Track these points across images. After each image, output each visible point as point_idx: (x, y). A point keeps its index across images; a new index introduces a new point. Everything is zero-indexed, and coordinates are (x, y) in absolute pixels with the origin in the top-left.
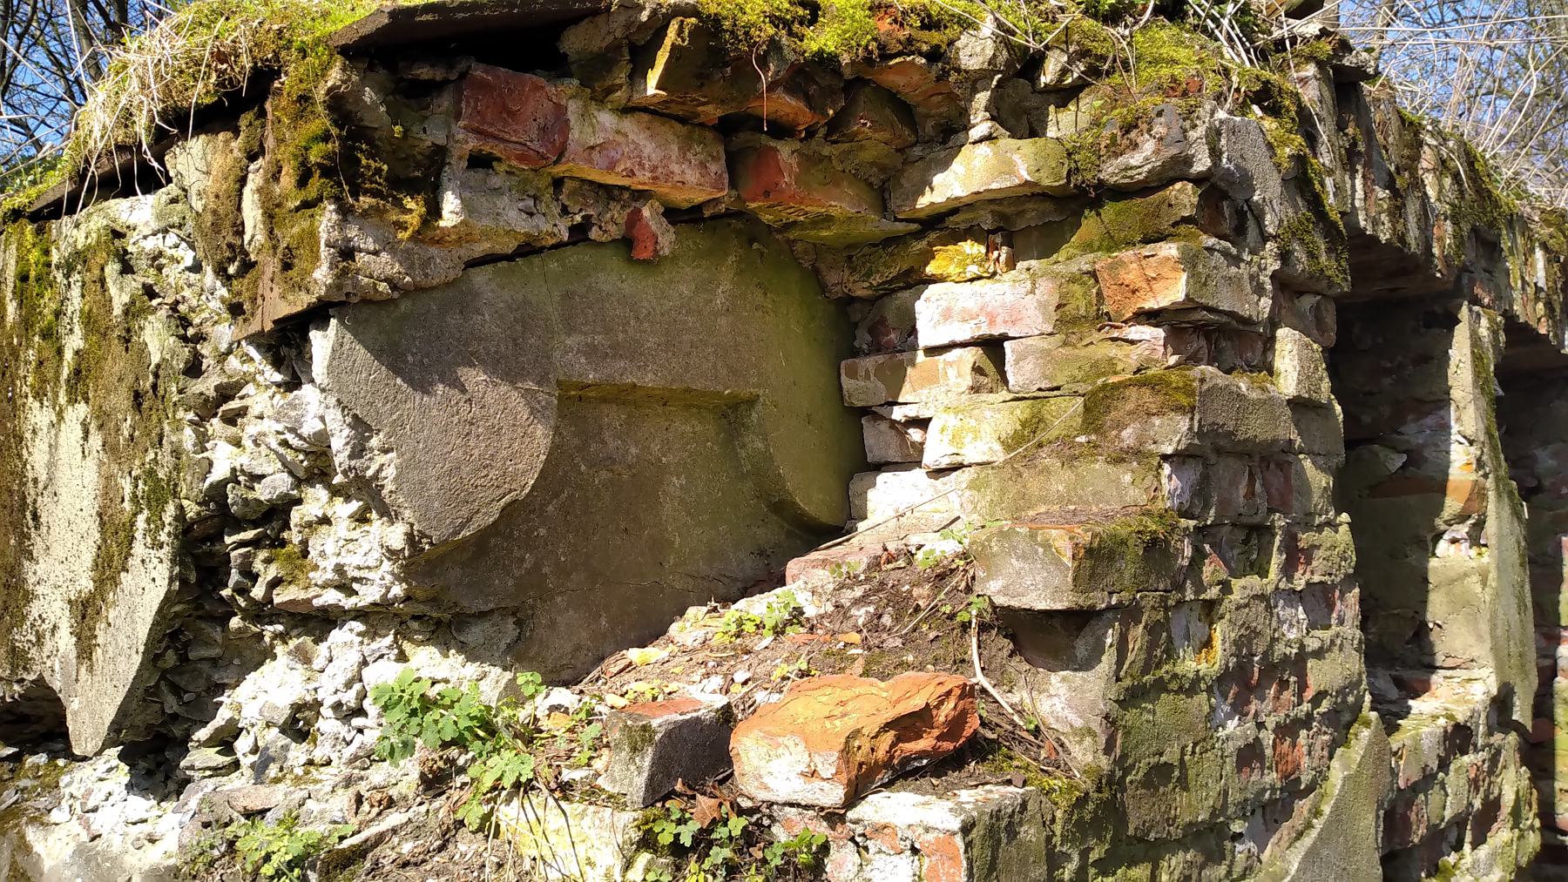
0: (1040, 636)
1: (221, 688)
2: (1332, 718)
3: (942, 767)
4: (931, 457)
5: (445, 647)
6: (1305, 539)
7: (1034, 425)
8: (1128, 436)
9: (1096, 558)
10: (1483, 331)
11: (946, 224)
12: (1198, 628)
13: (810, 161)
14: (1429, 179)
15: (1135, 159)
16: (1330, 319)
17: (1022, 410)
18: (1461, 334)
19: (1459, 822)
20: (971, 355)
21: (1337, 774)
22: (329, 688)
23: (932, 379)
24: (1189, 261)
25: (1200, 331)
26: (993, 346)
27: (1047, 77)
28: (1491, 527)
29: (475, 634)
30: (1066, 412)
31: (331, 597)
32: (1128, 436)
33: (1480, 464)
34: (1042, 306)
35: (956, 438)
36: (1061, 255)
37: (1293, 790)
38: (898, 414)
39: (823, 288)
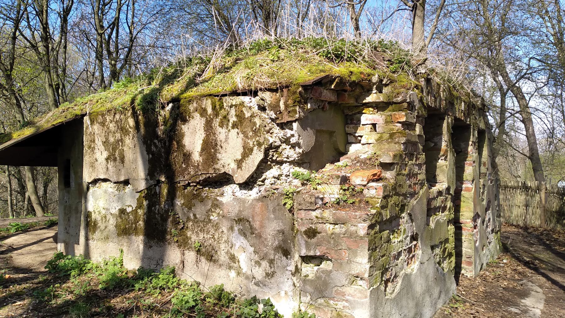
0: (386, 166)
2: (421, 184)
3: (377, 180)
4: (362, 142)
6: (419, 156)
8: (397, 140)
9: (395, 156)
11: (368, 105)
13: (349, 95)
14: (441, 93)
15: (399, 99)
16: (424, 122)
17: (379, 135)
18: (445, 121)
19: (439, 207)
20: (371, 126)
21: (421, 192)
22: (285, 172)
23: (363, 129)
24: (406, 115)
25: (408, 126)
27: (384, 82)
29: (305, 165)
30: (386, 136)
31: (285, 159)
32: (397, 140)
33: (447, 146)
34: (383, 119)
38: (357, 135)
39: (344, 113)
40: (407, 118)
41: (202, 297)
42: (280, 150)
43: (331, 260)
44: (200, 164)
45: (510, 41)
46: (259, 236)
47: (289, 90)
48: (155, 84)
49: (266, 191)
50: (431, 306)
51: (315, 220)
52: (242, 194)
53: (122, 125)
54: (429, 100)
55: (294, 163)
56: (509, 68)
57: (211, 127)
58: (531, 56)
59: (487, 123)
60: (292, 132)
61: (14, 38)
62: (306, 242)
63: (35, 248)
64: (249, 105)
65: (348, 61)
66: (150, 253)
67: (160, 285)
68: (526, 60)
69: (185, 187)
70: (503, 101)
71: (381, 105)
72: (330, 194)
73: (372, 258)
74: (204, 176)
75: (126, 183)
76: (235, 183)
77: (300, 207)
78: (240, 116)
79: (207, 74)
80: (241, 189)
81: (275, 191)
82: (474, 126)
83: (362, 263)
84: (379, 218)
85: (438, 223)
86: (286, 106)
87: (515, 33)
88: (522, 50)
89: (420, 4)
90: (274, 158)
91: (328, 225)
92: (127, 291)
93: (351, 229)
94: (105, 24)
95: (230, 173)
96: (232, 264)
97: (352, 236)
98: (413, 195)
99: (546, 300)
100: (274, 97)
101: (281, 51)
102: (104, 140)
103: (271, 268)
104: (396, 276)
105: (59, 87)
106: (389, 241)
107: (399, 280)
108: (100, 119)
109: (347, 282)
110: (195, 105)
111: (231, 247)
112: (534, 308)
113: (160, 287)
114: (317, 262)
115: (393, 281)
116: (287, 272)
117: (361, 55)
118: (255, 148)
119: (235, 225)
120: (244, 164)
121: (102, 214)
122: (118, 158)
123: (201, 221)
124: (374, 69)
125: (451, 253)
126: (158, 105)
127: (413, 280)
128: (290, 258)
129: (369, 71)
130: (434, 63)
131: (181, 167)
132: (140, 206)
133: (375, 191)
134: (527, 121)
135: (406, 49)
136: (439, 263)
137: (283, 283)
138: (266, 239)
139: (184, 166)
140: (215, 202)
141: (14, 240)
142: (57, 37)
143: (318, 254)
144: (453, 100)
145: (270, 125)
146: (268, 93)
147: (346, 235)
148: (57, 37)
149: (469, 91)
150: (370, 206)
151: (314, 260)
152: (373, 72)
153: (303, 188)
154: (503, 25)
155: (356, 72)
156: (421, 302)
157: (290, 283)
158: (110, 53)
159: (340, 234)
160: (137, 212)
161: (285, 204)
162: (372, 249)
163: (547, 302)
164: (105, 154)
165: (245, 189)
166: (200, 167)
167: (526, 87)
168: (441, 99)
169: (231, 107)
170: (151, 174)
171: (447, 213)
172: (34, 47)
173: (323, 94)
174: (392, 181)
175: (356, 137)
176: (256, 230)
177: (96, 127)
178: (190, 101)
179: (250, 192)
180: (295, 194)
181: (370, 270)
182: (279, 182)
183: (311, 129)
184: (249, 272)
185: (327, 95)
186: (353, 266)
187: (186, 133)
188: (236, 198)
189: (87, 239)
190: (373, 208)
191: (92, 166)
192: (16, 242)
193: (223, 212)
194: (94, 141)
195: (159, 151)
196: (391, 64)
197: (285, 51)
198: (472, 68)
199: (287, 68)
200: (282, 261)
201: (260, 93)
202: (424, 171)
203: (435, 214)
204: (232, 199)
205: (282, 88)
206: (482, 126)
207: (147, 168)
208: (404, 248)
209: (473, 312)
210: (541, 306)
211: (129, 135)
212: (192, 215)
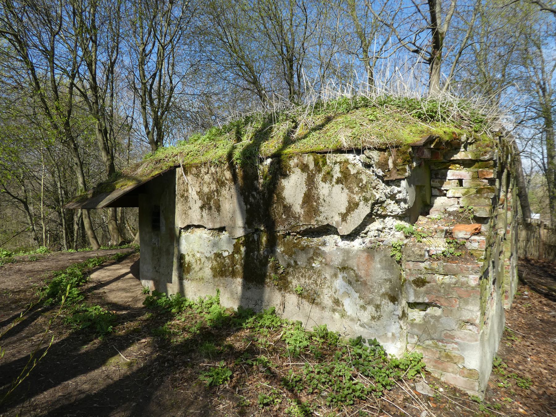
4: (447, 195)
8: (485, 195)
15: (486, 157)
17: (466, 190)
23: (449, 184)
29: (406, 219)
30: (474, 191)
31: (389, 214)
32: (485, 195)
36: (472, 168)
39: (430, 167)
42: (384, 205)
43: (439, 307)
44: (301, 216)
46: (365, 284)
49: (371, 242)
51: (424, 271)
52: (344, 244)
55: (400, 217)
57: (313, 182)
60: (399, 189)
62: (415, 290)
64: (353, 162)
66: (249, 294)
69: (285, 236)
71: (467, 162)
74: (306, 227)
75: (222, 229)
76: (338, 234)
77: (408, 259)
79: (299, 131)
81: (381, 243)
86: (395, 164)
90: (379, 212)
92: (235, 329)
93: (462, 279)
95: (334, 225)
96: (336, 307)
102: (199, 190)
103: (377, 312)
105: (107, 133)
108: (194, 170)
114: (423, 307)
116: (394, 316)
119: (339, 273)
120: (349, 218)
121: (196, 257)
122: (213, 207)
123: (302, 268)
126: (257, 160)
131: (281, 217)
132: (237, 250)
133: (477, 244)
137: (390, 325)
139: (284, 217)
140: (317, 251)
143: (427, 301)
145: (376, 181)
146: (376, 152)
147: (457, 285)
151: (420, 306)
153: (408, 240)
157: (397, 325)
160: (234, 256)
164: (199, 203)
165: (347, 240)
166: (302, 219)
169: (335, 163)
170: (249, 223)
175: (441, 191)
176: (362, 278)
178: (290, 158)
179: (353, 243)
180: (403, 247)
182: (382, 234)
184: (354, 315)
185: (427, 154)
189: (181, 279)
194: (187, 191)
195: (258, 202)
199: (389, 128)
200: (388, 306)
207: (245, 217)
211: (225, 186)
212: (292, 262)
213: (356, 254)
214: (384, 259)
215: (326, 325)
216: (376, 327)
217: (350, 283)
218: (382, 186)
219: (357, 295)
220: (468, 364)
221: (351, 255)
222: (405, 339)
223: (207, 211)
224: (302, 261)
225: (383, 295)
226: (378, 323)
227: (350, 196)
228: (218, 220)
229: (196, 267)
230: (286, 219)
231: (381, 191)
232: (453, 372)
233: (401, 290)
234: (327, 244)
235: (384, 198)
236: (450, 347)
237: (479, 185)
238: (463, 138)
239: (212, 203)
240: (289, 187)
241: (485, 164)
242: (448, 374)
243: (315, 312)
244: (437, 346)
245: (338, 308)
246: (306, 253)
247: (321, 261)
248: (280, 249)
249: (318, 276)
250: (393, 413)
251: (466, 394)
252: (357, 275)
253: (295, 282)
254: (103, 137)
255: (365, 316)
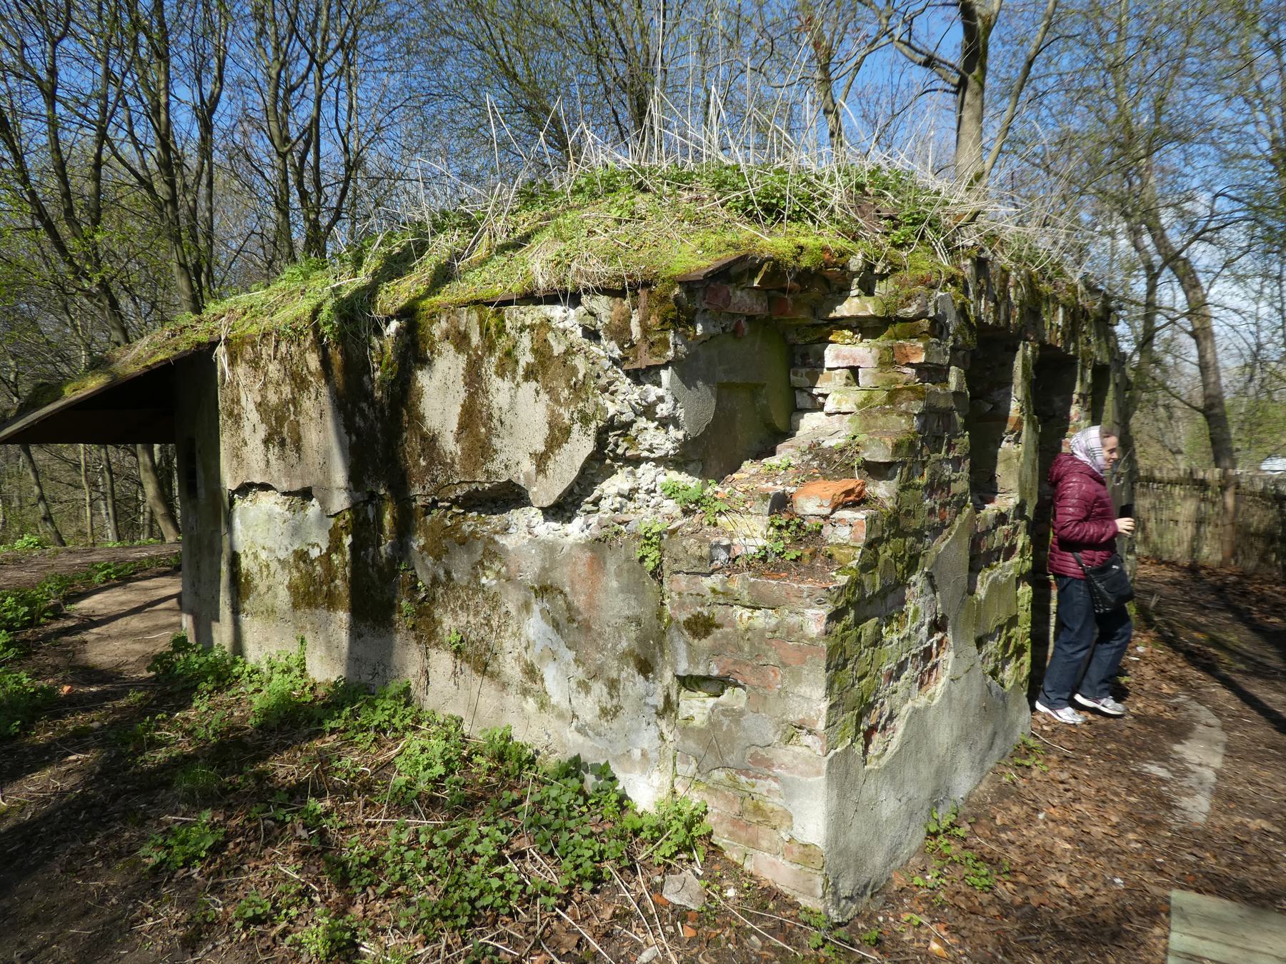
0: (877, 470)
1: (596, 484)
2: (957, 503)
4: (826, 409)
5: (680, 471)
6: (954, 441)
7: (869, 399)
8: (903, 407)
9: (897, 447)
10: (1029, 353)
11: (842, 323)
12: (920, 469)
13: (796, 301)
15: (910, 310)
16: (968, 359)
17: (864, 394)
18: (1019, 355)
19: (999, 550)
20: (846, 372)
21: (957, 522)
22: (645, 483)
23: (829, 379)
24: (926, 348)
26: (854, 370)
28: (1023, 437)
29: (691, 467)
30: (881, 396)
31: (645, 454)
32: (903, 407)
33: (1022, 410)
35: (839, 402)
36: (880, 339)
37: (943, 526)
38: (815, 391)
40: (928, 355)
41: (465, 753)
42: (633, 432)
44: (457, 460)
45: (1172, 155)
46: (586, 628)
47: (650, 292)
48: (363, 279)
49: (602, 526)
50: (972, 769)
52: (547, 530)
53: (294, 368)
54: (983, 309)
55: (663, 461)
56: (1166, 217)
58: (1217, 189)
59: (1114, 351)
60: (660, 392)
61: (98, 164)
62: (690, 645)
63: (135, 623)
64: (561, 325)
65: (794, 221)
67: (376, 723)
68: (1205, 197)
69: (428, 509)
70: (1152, 289)
71: (870, 324)
72: (747, 536)
73: (836, 686)
74: (466, 488)
75: (306, 494)
77: (676, 567)
78: (542, 352)
80: (546, 520)
81: (623, 527)
82: (1083, 360)
83: (811, 698)
84: (854, 594)
85: (995, 586)
86: (646, 330)
87: (1182, 139)
88: (1200, 182)
89: (975, 78)
90: (620, 451)
91: (739, 610)
92: (306, 731)
93: (789, 620)
94: (294, 134)
95: (522, 483)
96: (529, 684)
97: (792, 633)
98: (936, 531)
99: (1227, 747)
100: (617, 308)
101: (640, 197)
102: (259, 399)
103: (612, 697)
104: (891, 718)
106: (877, 641)
107: (900, 725)
108: (249, 353)
109: (778, 737)
110: (444, 324)
111: (526, 648)
112: (1200, 765)
113: (378, 726)
114: (714, 689)
115: (884, 728)
116: (646, 709)
117: (823, 206)
118: (576, 427)
119: (533, 600)
120: (550, 464)
122: (288, 440)
123: (461, 587)
124: (855, 239)
125: (1022, 645)
127: (930, 721)
128: (654, 679)
129: (842, 243)
130: (1001, 216)
131: (417, 464)
132: (335, 546)
133: (848, 529)
134: (1202, 335)
135: (935, 188)
136: (994, 673)
137: (638, 731)
138: (600, 634)
139: (423, 463)
140: (490, 547)
141: (97, 602)
142: (193, 161)
143: (715, 673)
144: (1039, 305)
145: (610, 373)
146: (604, 299)
147: (777, 634)
148: (193, 161)
149: (1076, 280)
150: (837, 567)
152: (850, 246)
153: (685, 520)
154: (1157, 122)
155: (811, 247)
156: (948, 764)
157: (653, 732)
158: (304, 196)
159: (764, 630)
160: (330, 559)
161: (642, 559)
162: (837, 662)
163: (1231, 751)
164: (262, 432)
165: (556, 520)
166: (457, 467)
167: (1203, 256)
168: (1009, 305)
169: (522, 329)
170: (355, 478)
171: (1017, 559)
172: (146, 184)
173: (734, 300)
174: (889, 504)
175: (814, 398)
176: (580, 613)
177: (241, 369)
179: (569, 528)
180: (665, 536)
181: (829, 714)
182: (631, 505)
183: (706, 382)
184: (565, 705)
186: (793, 703)
187: (425, 389)
188: (535, 540)
189: (236, 611)
190: (842, 569)
191: (236, 455)
192: (101, 606)
193: (508, 571)
194: (238, 402)
196: (896, 227)
197: (649, 196)
198: (1085, 216)
200: (635, 684)
201: (584, 298)
202: (966, 474)
203: (989, 566)
204: (526, 541)
205: (634, 288)
206: (1102, 357)
208: (914, 652)
209: (1064, 776)
210: (1217, 762)
212: (442, 572)
213: (569, 554)
214: (625, 566)
215: (510, 727)
216: (611, 736)
217: (556, 626)
218: (624, 384)
219: (571, 655)
220: (801, 831)
221: (559, 557)
222: (671, 765)
223: (276, 449)
224: (460, 566)
225: (623, 657)
226: (615, 724)
227: (553, 411)
228: (298, 472)
229: (261, 584)
230: (427, 469)
231: (621, 398)
232: (769, 850)
233: (661, 644)
234: (511, 530)
235: (628, 416)
236: (763, 786)
237: (896, 381)
238: (856, 263)
239: (286, 429)
240: (432, 390)
241: (909, 327)
242: (760, 854)
243: (487, 696)
244: (735, 785)
245: (534, 686)
246: (470, 551)
247: (499, 572)
248: (418, 542)
249: (494, 608)
250: (564, 951)
251: (795, 906)
252: (569, 607)
253: (448, 622)
254: (190, 280)
255: (588, 708)
